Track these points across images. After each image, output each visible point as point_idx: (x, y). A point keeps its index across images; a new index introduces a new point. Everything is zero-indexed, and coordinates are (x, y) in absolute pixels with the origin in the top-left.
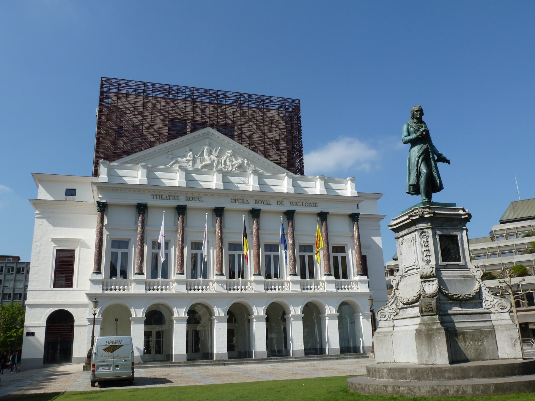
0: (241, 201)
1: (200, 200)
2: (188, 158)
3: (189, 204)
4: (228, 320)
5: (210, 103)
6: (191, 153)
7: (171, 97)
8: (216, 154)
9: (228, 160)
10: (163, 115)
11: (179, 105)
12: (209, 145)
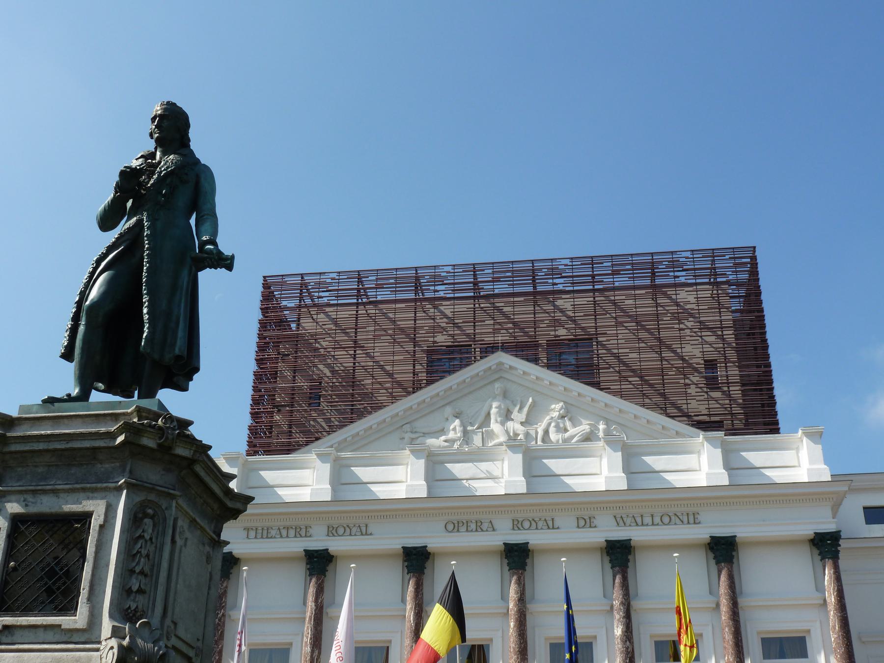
0: (473, 526)
1: (365, 532)
2: (451, 435)
3: (335, 545)
5: (635, 288)
6: (457, 422)
7: (658, 281)
8: (522, 417)
9: (552, 430)
10: (644, 328)
11: (559, 303)
12: (505, 395)
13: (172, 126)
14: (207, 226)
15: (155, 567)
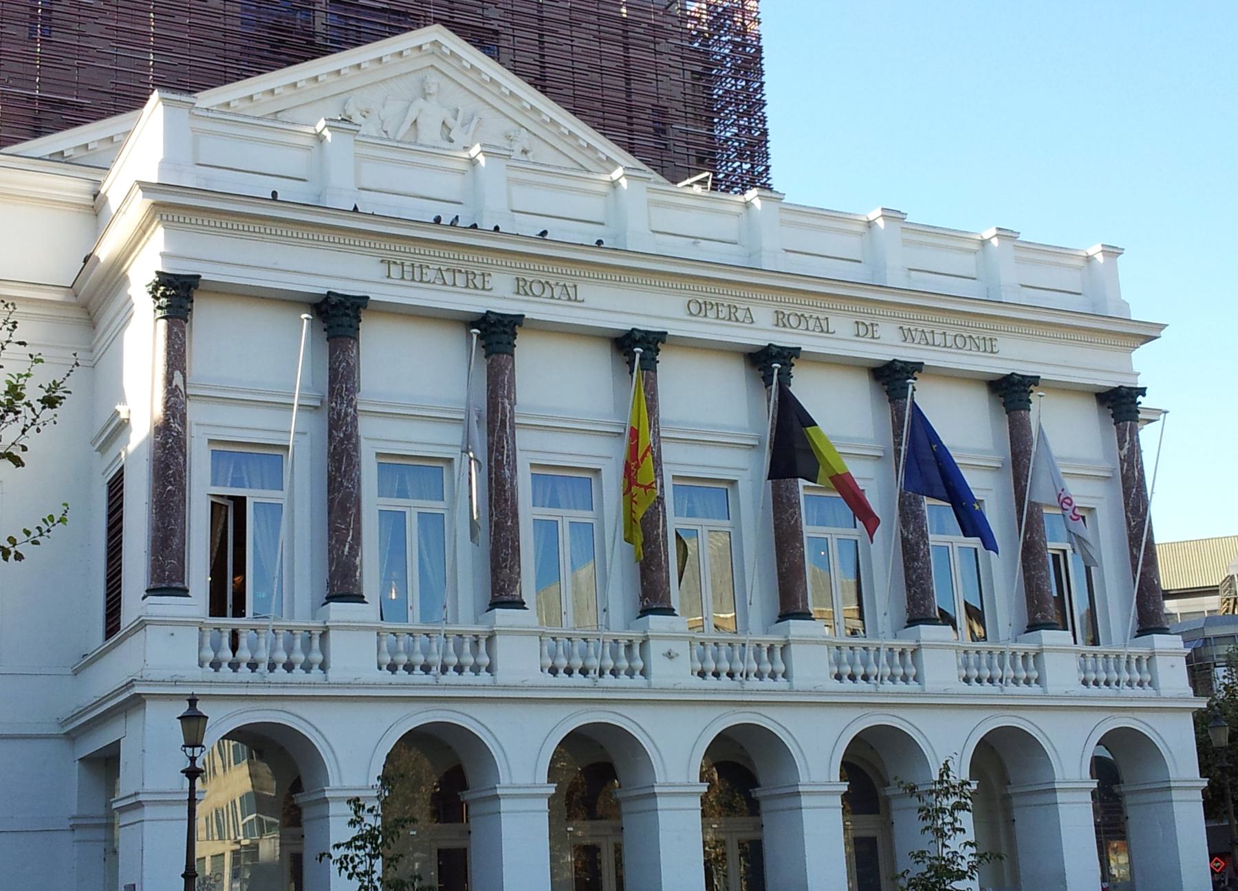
0: (724, 313)
4: (845, 797)
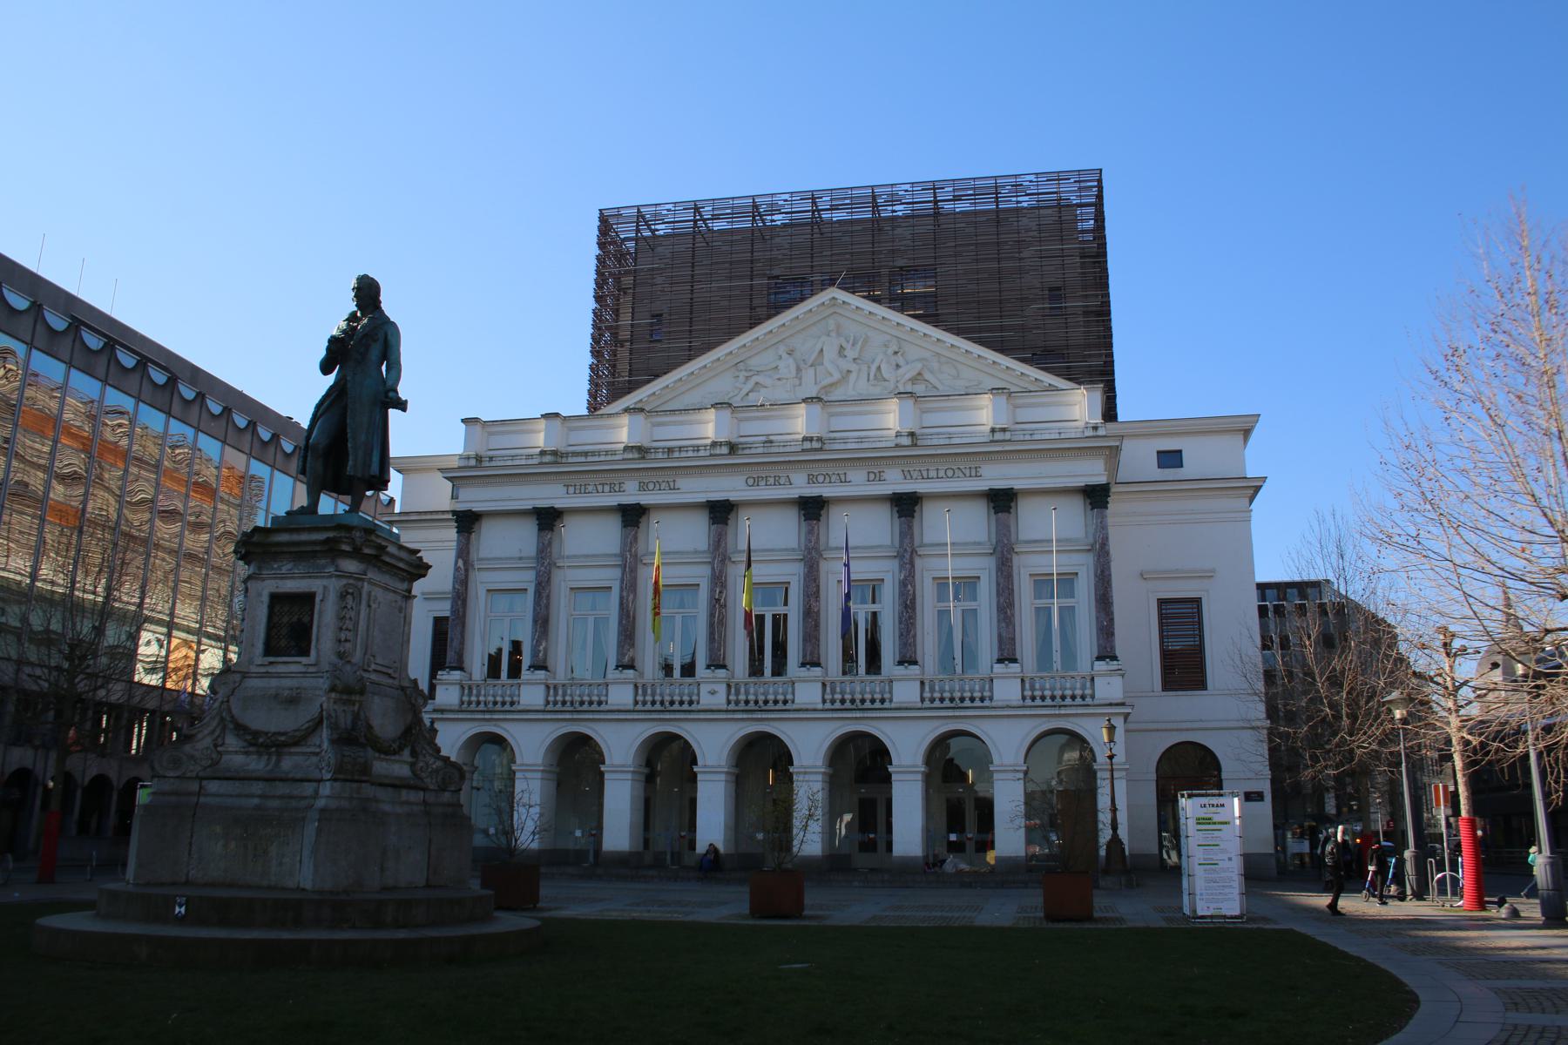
0: (771, 480)
13: (367, 292)
14: (393, 372)
15: (356, 624)
